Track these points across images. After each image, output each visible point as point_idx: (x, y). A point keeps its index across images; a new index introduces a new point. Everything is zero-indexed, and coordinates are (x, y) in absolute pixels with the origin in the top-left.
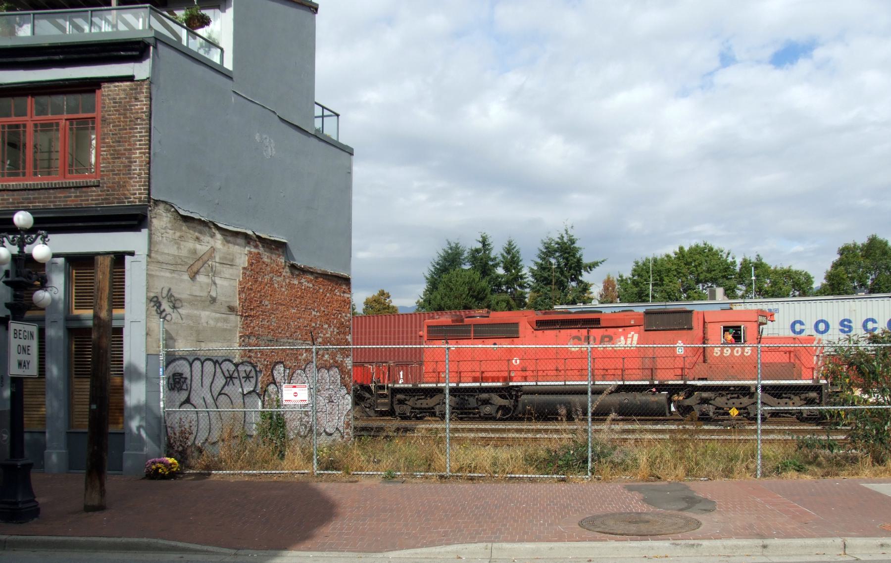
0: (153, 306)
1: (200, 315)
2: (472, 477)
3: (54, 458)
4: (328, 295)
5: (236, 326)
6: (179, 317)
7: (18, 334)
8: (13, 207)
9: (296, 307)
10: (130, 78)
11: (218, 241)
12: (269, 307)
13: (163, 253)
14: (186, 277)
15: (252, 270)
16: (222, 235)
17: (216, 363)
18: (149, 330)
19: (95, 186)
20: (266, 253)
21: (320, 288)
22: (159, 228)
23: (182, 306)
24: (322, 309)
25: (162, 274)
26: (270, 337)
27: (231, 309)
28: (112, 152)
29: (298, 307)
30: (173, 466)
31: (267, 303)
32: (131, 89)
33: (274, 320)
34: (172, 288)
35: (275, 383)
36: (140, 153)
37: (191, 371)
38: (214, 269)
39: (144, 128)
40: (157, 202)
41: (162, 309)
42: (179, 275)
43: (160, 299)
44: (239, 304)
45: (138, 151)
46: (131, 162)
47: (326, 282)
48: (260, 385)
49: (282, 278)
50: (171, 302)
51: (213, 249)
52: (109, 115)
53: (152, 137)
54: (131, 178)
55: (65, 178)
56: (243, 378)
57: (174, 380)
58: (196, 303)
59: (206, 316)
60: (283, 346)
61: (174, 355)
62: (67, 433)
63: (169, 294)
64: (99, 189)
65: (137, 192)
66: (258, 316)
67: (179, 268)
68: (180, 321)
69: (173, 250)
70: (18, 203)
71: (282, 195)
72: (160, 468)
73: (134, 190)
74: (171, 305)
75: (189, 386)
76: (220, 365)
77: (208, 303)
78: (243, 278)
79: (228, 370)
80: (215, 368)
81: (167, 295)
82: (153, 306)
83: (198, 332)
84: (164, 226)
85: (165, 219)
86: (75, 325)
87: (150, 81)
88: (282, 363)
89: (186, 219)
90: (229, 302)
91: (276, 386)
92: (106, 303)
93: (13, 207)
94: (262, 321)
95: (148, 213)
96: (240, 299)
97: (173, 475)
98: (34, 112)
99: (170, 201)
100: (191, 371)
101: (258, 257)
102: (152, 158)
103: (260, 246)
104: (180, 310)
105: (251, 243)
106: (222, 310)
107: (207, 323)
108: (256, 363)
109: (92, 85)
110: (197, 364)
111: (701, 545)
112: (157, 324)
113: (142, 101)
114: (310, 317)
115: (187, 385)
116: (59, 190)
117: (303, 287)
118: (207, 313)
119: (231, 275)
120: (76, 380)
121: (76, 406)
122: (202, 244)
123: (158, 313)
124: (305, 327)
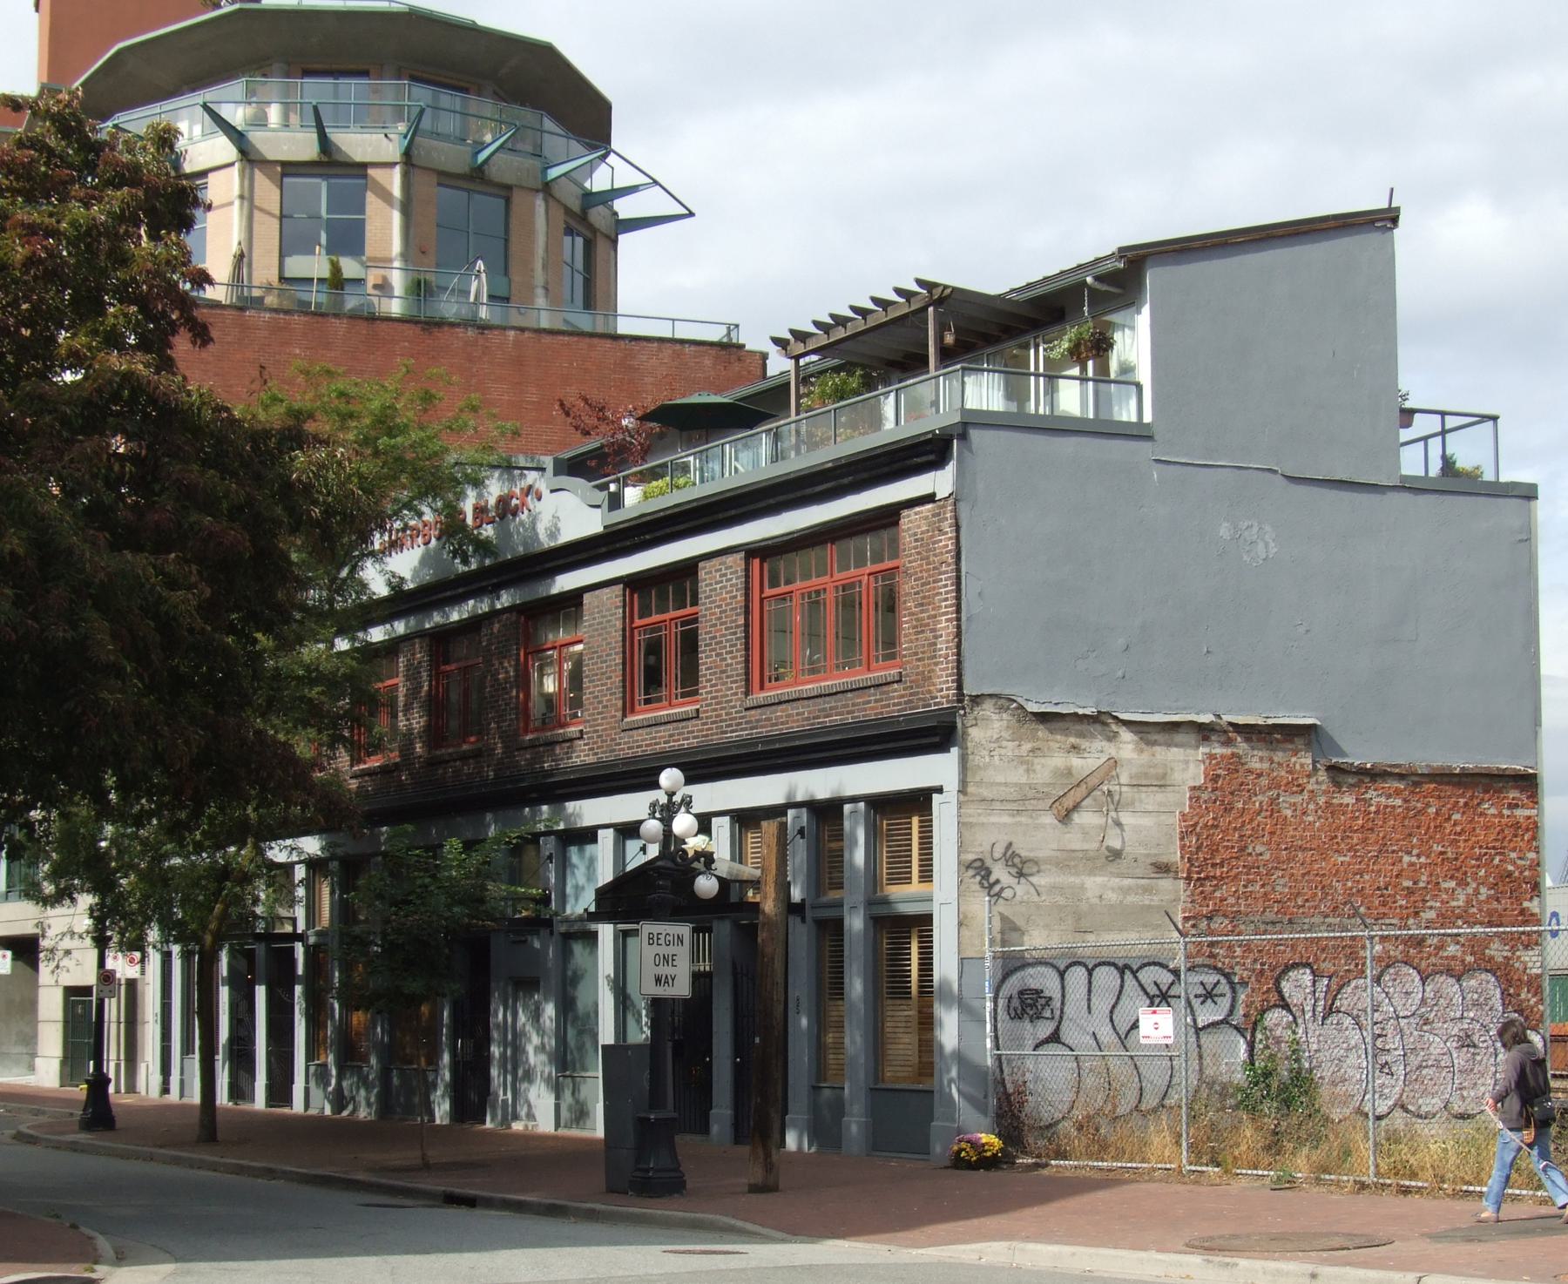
0: (974, 876)
1: (1083, 884)
2: (1408, 1187)
3: (854, 1128)
4: (1456, 817)
5: (1177, 900)
6: (1032, 890)
7: (655, 939)
8: (808, 725)
9: (1349, 850)
10: (929, 498)
11: (1127, 746)
12: (1267, 856)
13: (993, 784)
14: (1049, 819)
15: (1214, 790)
16: (1136, 733)
17: (1122, 970)
18: (966, 917)
19: (897, 682)
20: (1255, 752)
21: (1428, 805)
22: (983, 742)
23: (1038, 872)
24: (1437, 848)
25: (993, 819)
26: (1270, 916)
27: (1163, 869)
28: (914, 623)
29: (1356, 851)
30: (986, 1147)
31: (1259, 849)
32: (933, 516)
33: (1282, 881)
34: (1014, 840)
35: (1286, 1006)
36: (947, 620)
37: (1063, 988)
38: (1116, 798)
39: (950, 578)
40: (977, 700)
41: (992, 879)
42: (1031, 817)
43: (989, 863)
44: (1182, 858)
45: (944, 618)
46: (936, 637)
47: (1448, 790)
48: (1240, 1011)
49: (1306, 795)
50: (1014, 865)
51: (1114, 763)
52: (910, 562)
53: (963, 592)
54: (936, 664)
55: (869, 670)
56: (1196, 996)
57: (1022, 1002)
58: (1073, 863)
59: (1098, 886)
60: (1310, 931)
61: (1023, 958)
62: (871, 1089)
63: (1010, 852)
64: (902, 686)
65: (944, 686)
66: (1236, 877)
67: (1029, 805)
68: (1036, 898)
69: (1018, 776)
70: (814, 718)
71: (1301, 630)
72: (964, 1149)
73: (940, 683)
74: (1014, 871)
75: (1058, 1013)
76: (1134, 973)
77: (1104, 860)
78: (1190, 807)
79: (1155, 983)
80: (1123, 981)
81: (1005, 854)
82: (974, 876)
83: (1078, 917)
84: (995, 736)
85: (997, 725)
86: (882, 911)
87: (955, 498)
88: (1308, 965)
89: (1044, 718)
90: (1156, 855)
91: (1290, 1011)
92: (772, 890)
93: (808, 725)
94: (1245, 886)
95: (959, 721)
96: (1183, 847)
97: (989, 1163)
98: (835, 566)
99: (1007, 691)
100: (1063, 988)
101: (1235, 764)
102: (963, 627)
103: (1239, 739)
104: (1034, 879)
105: (1213, 738)
106: (1138, 870)
107: (1101, 897)
108: (1232, 968)
109: (888, 516)
110: (1077, 976)
111: (1237, 1265)
112: (980, 905)
113: (946, 533)
114: (1396, 869)
115: (1052, 1010)
116: (856, 693)
117: (1373, 809)
118: (1099, 880)
119: (1160, 804)
120: (890, 1002)
121: (889, 1046)
122: (1086, 755)
123: (983, 887)
124: (1379, 889)
